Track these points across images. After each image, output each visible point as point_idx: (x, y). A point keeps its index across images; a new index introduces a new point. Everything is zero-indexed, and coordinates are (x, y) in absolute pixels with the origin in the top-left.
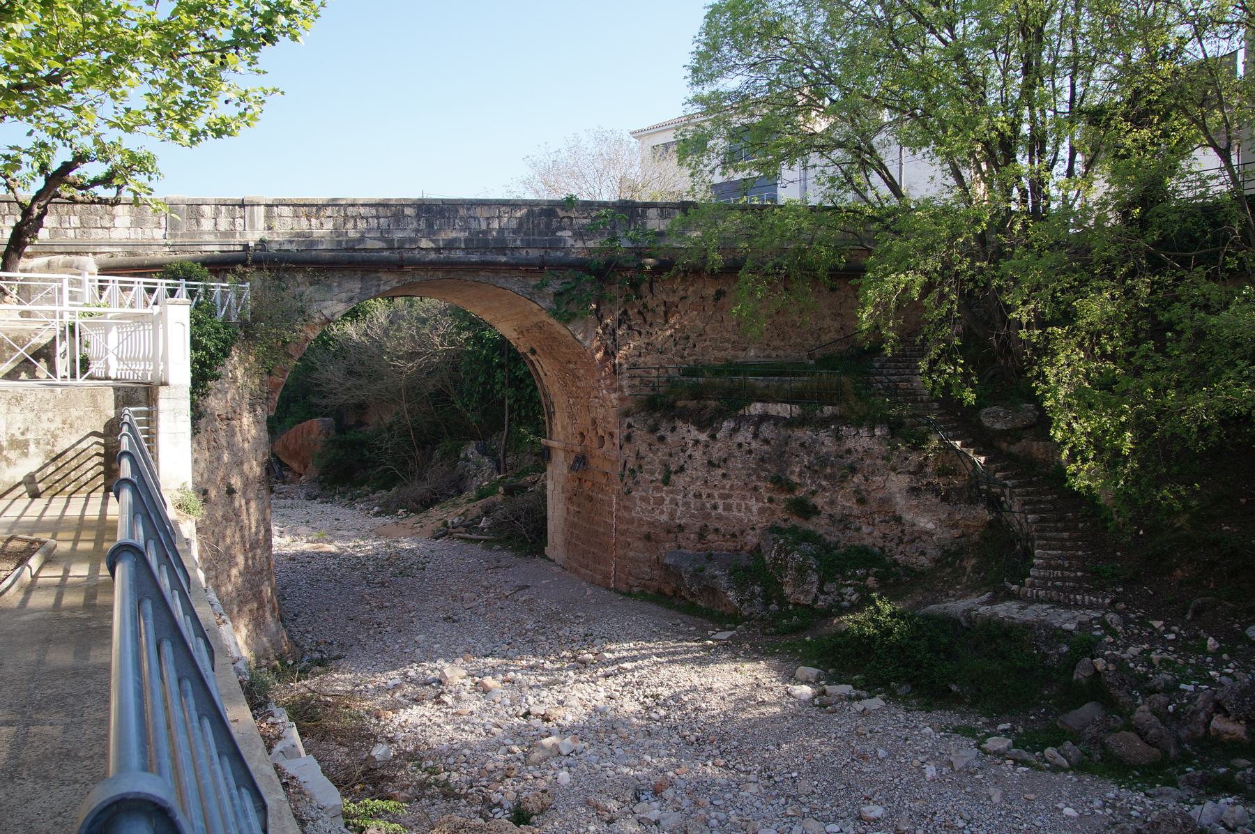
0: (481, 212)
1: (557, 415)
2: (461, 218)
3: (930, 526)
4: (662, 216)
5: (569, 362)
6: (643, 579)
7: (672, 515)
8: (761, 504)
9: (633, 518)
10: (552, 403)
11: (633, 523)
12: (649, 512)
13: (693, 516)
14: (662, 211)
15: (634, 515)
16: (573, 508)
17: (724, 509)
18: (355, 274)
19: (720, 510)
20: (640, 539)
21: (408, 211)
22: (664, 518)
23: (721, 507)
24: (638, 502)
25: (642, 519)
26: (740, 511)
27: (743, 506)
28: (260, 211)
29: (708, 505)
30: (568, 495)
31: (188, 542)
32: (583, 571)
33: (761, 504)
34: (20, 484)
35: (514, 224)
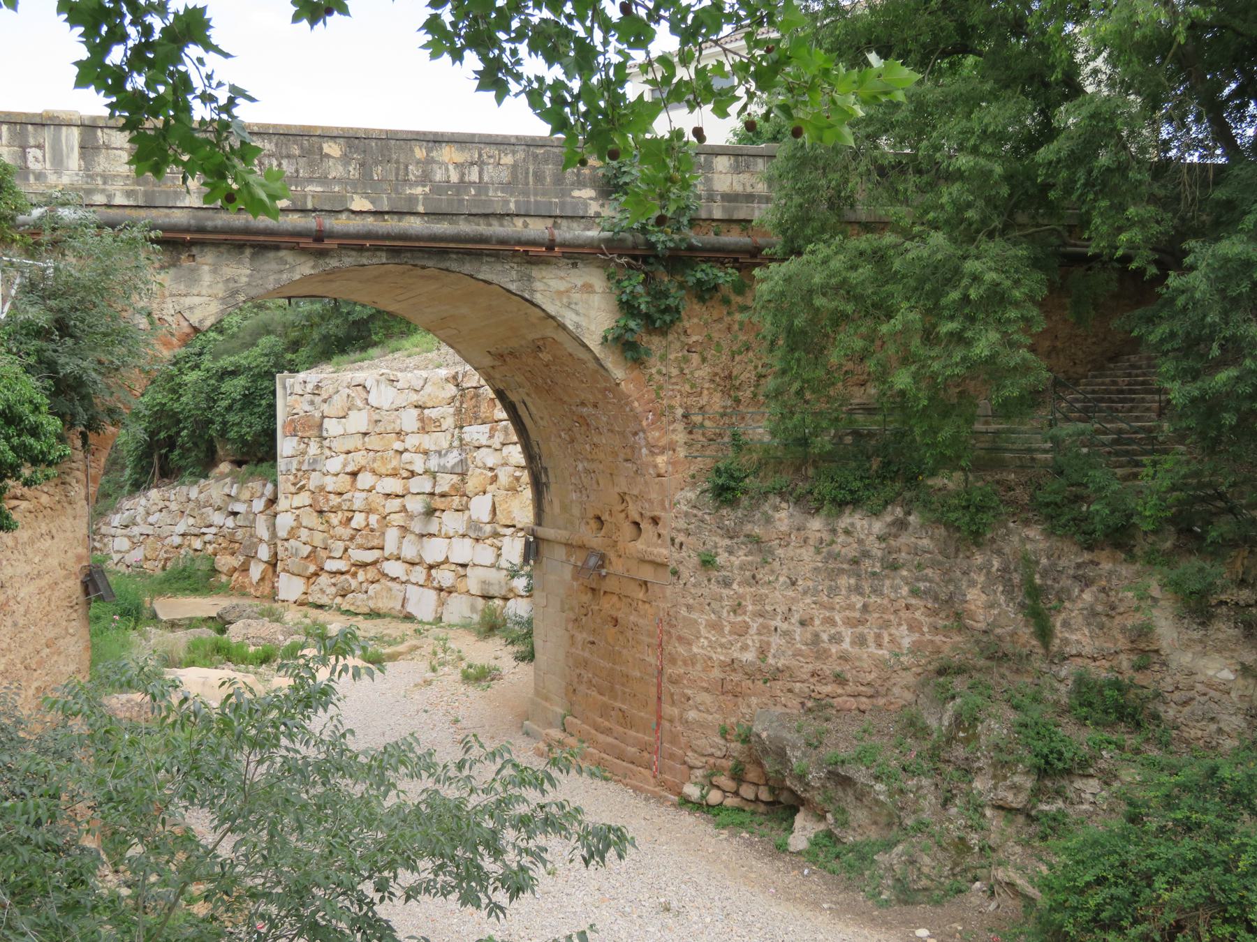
0: (448, 154)
1: (553, 487)
2: (418, 162)
3: (1227, 675)
4: (737, 170)
5: (583, 404)
6: (712, 755)
7: (763, 652)
8: (916, 636)
9: (695, 655)
10: (546, 469)
11: (693, 664)
12: (722, 646)
13: (796, 654)
14: (736, 161)
15: (695, 650)
16: (581, 637)
17: (853, 643)
18: (242, 253)
19: (846, 645)
20: (707, 690)
21: (333, 149)
22: (749, 656)
23: (848, 640)
24: (703, 632)
25: (710, 658)
26: (880, 646)
27: (886, 639)
28: (73, 137)
29: (825, 637)
30: (572, 616)
31: (255, 216)
32: (602, 738)
33: (916, 636)
34: (543, 310)
35: (505, 176)
